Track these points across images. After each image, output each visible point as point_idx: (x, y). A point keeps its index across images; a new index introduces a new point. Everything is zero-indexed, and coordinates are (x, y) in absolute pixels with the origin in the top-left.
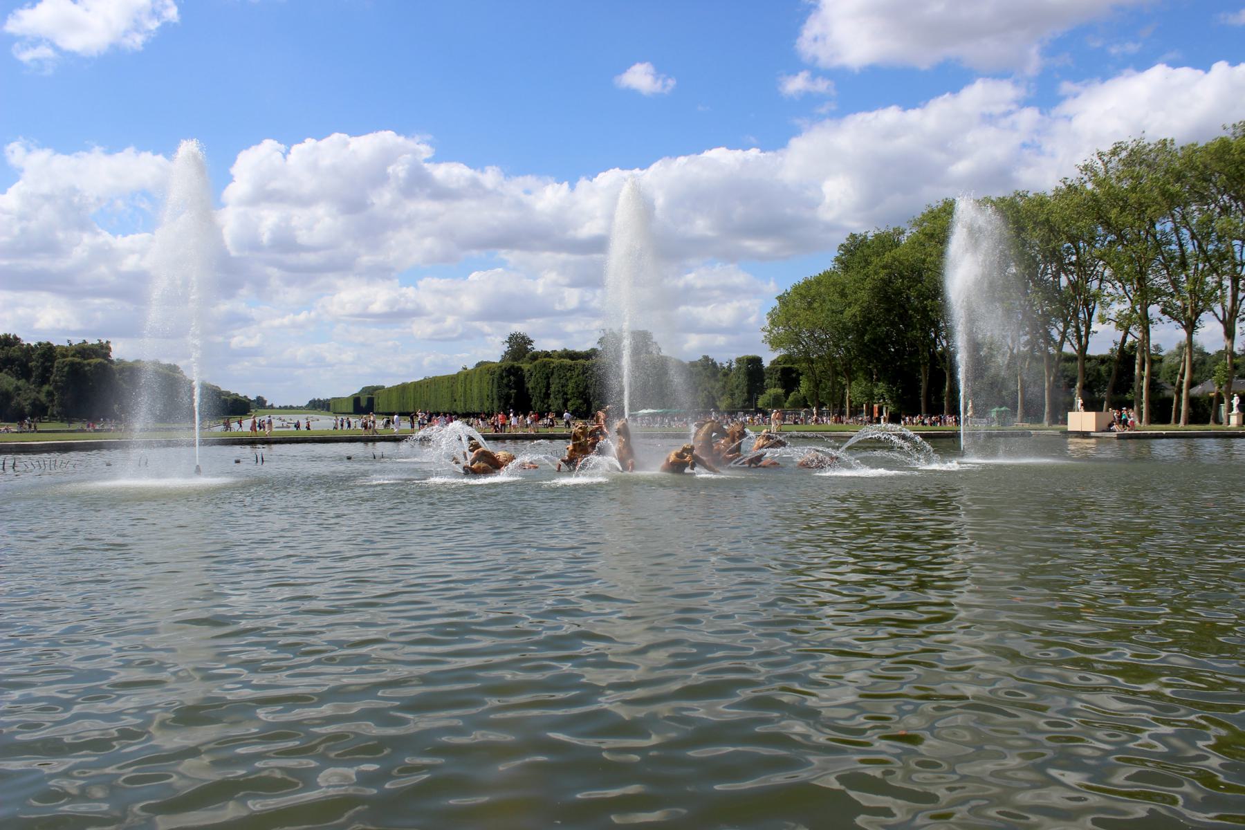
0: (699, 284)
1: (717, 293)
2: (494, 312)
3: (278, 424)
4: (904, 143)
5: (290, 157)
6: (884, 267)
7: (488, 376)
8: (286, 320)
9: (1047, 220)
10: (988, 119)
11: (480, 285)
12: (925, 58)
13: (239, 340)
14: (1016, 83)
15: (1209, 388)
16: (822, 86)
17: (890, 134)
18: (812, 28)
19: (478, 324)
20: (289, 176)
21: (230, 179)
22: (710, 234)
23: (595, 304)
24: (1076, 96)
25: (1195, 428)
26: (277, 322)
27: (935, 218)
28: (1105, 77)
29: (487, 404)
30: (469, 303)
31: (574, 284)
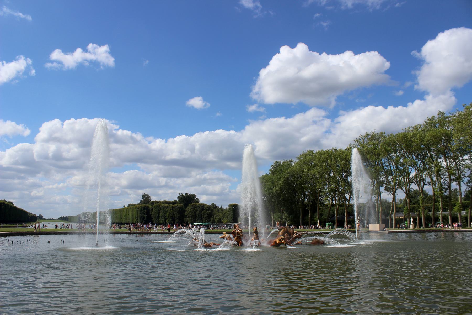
0: (208, 177)
1: (215, 181)
2: (134, 186)
3: (51, 226)
4: (285, 129)
5: (64, 126)
6: (288, 173)
7: (136, 210)
8: (55, 186)
9: (345, 158)
10: (315, 122)
11: (127, 177)
12: (295, 101)
13: (34, 193)
14: (325, 110)
15: (401, 216)
16: (262, 110)
17: (281, 126)
18: (256, 89)
19: (126, 190)
20: (57, 133)
21: (39, 132)
22: (215, 160)
23: (171, 184)
24: (344, 115)
25: (397, 230)
26: (51, 187)
27: (305, 156)
28: (354, 109)
29: (135, 220)
30: (124, 182)
31: (164, 176)
